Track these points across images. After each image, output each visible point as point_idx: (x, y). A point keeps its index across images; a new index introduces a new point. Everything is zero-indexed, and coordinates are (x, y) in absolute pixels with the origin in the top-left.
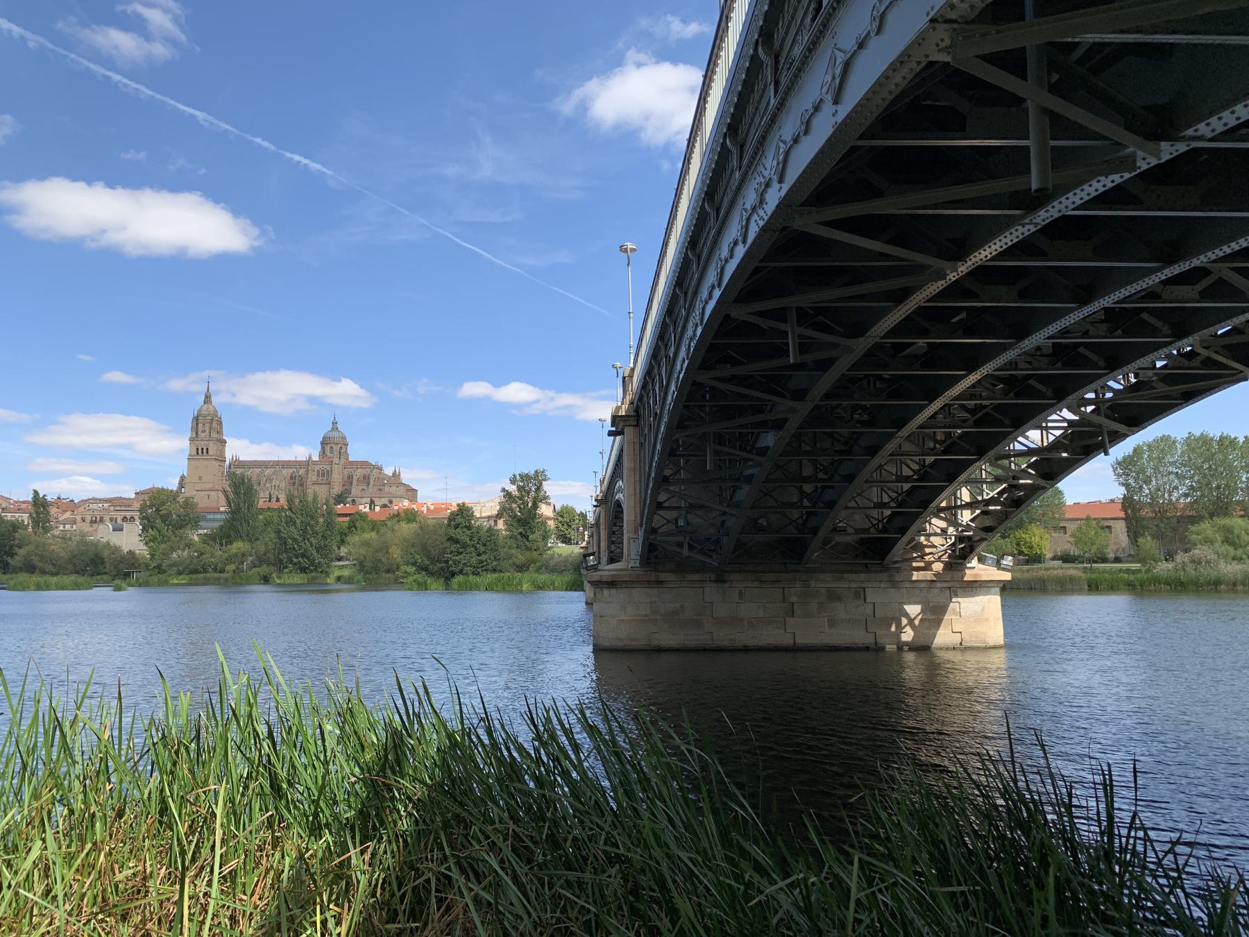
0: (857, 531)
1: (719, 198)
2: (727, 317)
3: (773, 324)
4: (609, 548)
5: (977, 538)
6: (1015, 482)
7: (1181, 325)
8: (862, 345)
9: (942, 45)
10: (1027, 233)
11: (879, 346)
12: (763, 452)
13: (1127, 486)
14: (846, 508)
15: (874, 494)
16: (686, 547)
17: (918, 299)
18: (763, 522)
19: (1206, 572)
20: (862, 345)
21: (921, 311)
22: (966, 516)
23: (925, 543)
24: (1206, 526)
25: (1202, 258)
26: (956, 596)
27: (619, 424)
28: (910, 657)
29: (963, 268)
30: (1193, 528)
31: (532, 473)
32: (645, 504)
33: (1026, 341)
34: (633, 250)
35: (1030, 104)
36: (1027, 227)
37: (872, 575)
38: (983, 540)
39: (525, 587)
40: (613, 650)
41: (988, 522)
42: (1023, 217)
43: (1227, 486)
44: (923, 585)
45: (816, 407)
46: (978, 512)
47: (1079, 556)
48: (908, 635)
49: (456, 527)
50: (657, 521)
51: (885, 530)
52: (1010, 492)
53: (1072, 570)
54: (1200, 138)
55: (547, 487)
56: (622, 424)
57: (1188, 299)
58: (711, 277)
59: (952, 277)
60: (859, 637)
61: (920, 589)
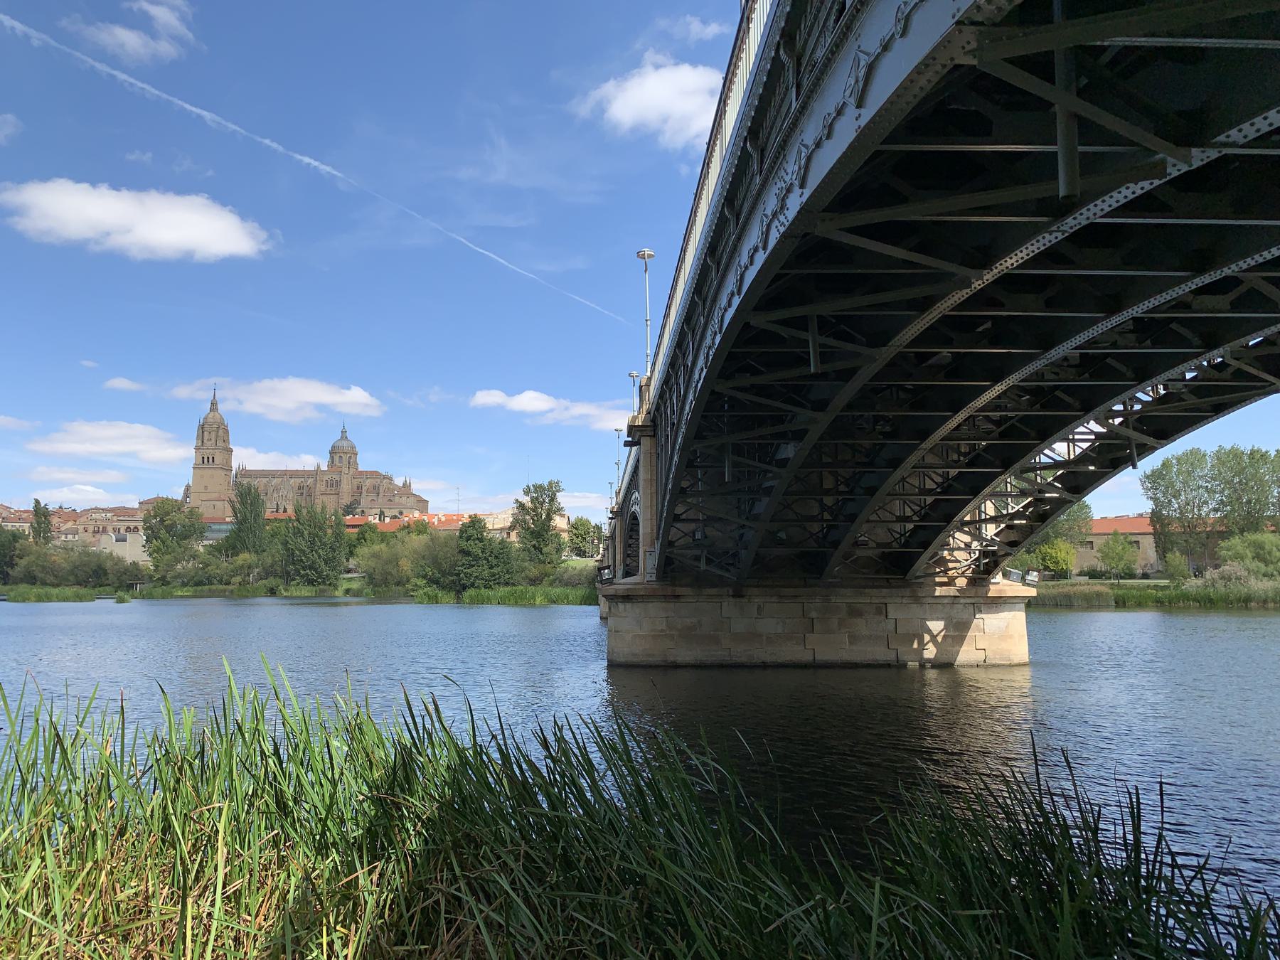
0: (879, 545)
2: (747, 325)
4: (624, 561)
5: (1002, 553)
6: (1041, 496)
7: (1211, 336)
8: (886, 353)
9: (968, 48)
11: (901, 356)
12: (783, 463)
13: (1155, 499)
14: (868, 521)
15: (896, 507)
16: (703, 560)
17: (944, 307)
18: (782, 535)
19: (1236, 589)
20: (886, 353)
21: (944, 319)
22: (990, 530)
23: (948, 558)
24: (1236, 541)
25: (1233, 267)
26: (980, 612)
27: (635, 434)
28: (931, 674)
29: (989, 277)
31: (546, 484)
34: (650, 256)
36: (1055, 234)
38: (1008, 555)
39: (538, 601)
41: (1013, 536)
42: (1049, 224)
43: (1258, 501)
44: (946, 601)
46: (1003, 526)
48: (930, 652)
49: (468, 539)
50: (674, 534)
51: (906, 545)
53: (1099, 586)
54: (1234, 145)
55: (561, 497)
56: (638, 434)
57: (1220, 309)
59: (977, 285)
60: (880, 653)
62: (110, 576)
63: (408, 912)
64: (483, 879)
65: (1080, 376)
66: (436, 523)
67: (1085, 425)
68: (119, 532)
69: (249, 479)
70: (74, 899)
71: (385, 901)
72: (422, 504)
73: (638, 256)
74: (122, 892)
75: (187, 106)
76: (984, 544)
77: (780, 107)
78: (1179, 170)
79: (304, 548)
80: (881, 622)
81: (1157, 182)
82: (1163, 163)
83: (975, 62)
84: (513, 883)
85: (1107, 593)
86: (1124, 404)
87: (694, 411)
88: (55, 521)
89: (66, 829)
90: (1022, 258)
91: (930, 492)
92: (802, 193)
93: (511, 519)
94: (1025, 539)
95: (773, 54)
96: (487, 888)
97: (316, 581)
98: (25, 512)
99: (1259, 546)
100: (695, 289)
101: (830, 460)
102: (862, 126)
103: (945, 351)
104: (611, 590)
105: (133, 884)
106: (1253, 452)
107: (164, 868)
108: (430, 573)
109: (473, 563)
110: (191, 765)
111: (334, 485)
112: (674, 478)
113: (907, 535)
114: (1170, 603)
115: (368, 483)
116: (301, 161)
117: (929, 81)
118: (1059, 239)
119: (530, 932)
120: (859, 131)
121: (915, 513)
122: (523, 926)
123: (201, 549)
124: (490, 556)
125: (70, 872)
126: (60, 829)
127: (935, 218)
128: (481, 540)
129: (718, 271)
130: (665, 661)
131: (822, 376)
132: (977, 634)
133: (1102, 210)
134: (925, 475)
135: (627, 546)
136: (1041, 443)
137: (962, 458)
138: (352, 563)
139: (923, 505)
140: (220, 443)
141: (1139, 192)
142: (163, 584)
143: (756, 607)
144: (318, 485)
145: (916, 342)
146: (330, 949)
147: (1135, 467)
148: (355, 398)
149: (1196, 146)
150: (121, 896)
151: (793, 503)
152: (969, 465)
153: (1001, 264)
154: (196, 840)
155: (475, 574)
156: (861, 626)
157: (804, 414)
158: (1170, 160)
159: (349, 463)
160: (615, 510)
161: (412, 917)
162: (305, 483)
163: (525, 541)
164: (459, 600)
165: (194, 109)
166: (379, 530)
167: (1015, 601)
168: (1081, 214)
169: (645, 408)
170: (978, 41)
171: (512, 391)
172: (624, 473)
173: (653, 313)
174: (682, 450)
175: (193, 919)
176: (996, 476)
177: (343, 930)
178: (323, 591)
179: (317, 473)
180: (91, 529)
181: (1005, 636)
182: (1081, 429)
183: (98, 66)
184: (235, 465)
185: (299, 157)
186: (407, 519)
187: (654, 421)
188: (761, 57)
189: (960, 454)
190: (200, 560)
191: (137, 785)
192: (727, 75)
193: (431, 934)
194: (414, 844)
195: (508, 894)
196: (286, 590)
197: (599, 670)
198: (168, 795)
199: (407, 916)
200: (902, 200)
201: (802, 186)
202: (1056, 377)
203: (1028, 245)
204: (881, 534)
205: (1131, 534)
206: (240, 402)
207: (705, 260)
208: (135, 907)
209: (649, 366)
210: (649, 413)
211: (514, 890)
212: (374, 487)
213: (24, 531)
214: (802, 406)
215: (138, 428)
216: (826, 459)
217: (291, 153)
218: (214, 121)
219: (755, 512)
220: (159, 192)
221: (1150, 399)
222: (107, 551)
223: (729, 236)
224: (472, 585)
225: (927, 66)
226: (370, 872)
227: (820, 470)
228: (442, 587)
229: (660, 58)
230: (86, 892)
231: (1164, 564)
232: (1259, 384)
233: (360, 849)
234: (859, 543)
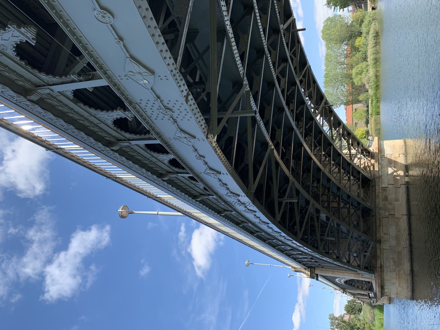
0: (359, 188)
1: (239, 221)
2: (279, 222)
3: (283, 207)
5: (362, 148)
6: (341, 135)
7: (292, 83)
8: (291, 178)
9: (213, 137)
10: (263, 123)
11: (292, 174)
12: (328, 218)
13: (340, 104)
14: (350, 191)
15: (344, 182)
16: (365, 254)
17: (278, 158)
18: (355, 223)
19: (373, 79)
20: (291, 178)
21: (282, 158)
22: (353, 151)
23: (363, 165)
24: (355, 81)
25: (274, 76)
26: (384, 155)
27: (314, 276)
28: (411, 173)
29: (271, 143)
30: (356, 84)
31: (330, 320)
32: (347, 269)
33: (294, 128)
34: (248, 262)
35: (230, 116)
36: (261, 123)
37: (376, 184)
38: (362, 145)
40: (413, 291)
41: (356, 144)
42: (258, 124)
43: (341, 75)
45: (312, 197)
46: (352, 147)
47: (366, 119)
48: (401, 173)
50: (355, 264)
51: (359, 179)
52: (345, 136)
53: (372, 120)
54: (244, 73)
55: (337, 315)
56: (314, 274)
57: (285, 81)
58: (264, 227)
59: (273, 147)
60: (402, 191)
61: (382, 168)
92: (241, 196)
99: (357, 74)
106: (325, 77)
121: (347, 175)
130: (410, 274)
132: (393, 157)
139: (344, 173)
143: (384, 235)
149: (243, 83)
151: (343, 218)
156: (391, 197)
157: (311, 209)
160: (342, 291)
167: (380, 143)
170: (212, 134)
182: (319, 121)
187: (309, 267)
204: (355, 188)
205: (352, 111)
210: (305, 269)
214: (307, 210)
219: (346, 232)
227: (331, 208)
232: (307, 71)
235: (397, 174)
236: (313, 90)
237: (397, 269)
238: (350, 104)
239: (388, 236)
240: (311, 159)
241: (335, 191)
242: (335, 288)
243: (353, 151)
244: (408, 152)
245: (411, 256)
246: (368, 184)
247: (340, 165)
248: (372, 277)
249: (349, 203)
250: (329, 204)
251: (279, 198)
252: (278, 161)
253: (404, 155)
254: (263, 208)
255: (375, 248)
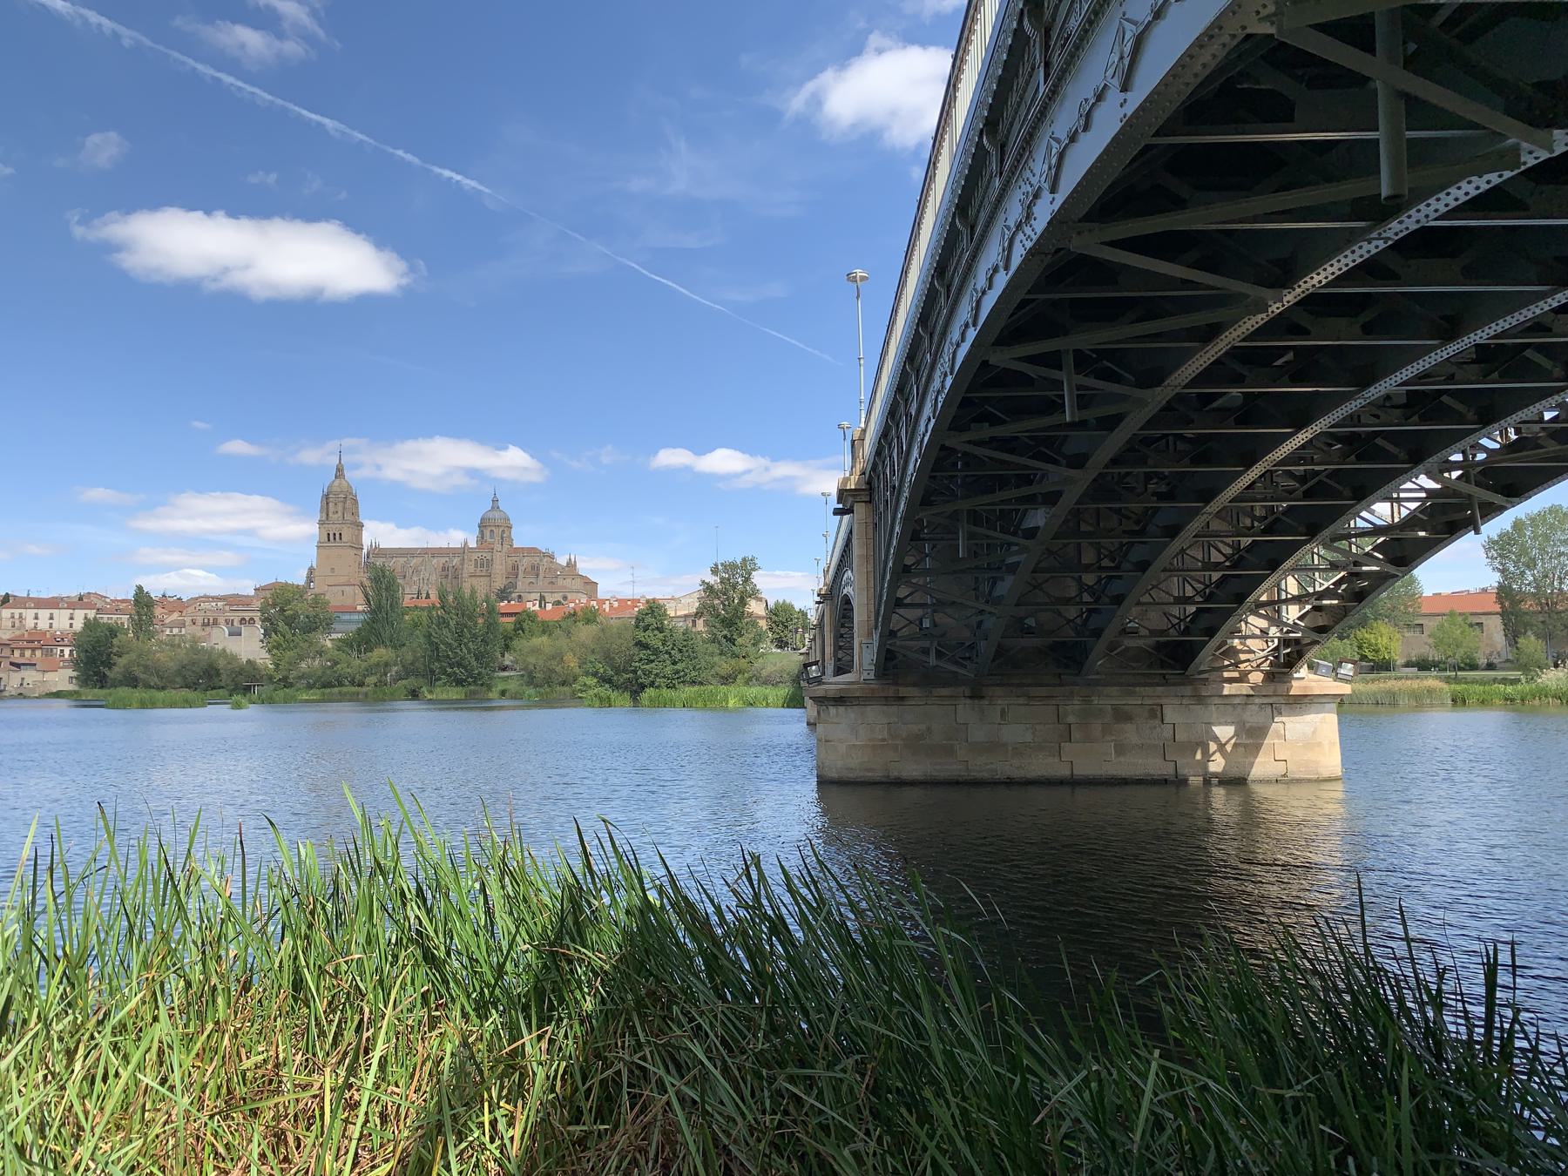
0: (1153, 633)
2: (985, 364)
5: (1307, 641)
6: (1356, 569)
9: (1264, 12)
10: (1374, 251)
11: (1179, 398)
12: (1032, 533)
13: (1503, 571)
14: (1139, 603)
15: (1174, 586)
18: (1031, 622)
21: (1234, 353)
23: (1239, 647)
26: (1280, 714)
27: (847, 501)
28: (1219, 794)
29: (1290, 298)
34: (863, 279)
36: (1375, 243)
39: (731, 703)
41: (1321, 620)
42: (1369, 230)
44: (1237, 701)
46: (1308, 607)
48: (1217, 765)
49: (646, 629)
50: (896, 622)
51: (1187, 632)
55: (758, 579)
56: (850, 499)
59: (1275, 308)
60: (1155, 766)
61: (1233, 705)
62: (224, 677)
63: (584, 1084)
64: (673, 1046)
65: (1406, 419)
66: (607, 610)
67: (1414, 480)
68: (232, 625)
69: (384, 560)
70: (193, 1067)
71: (556, 1071)
72: (590, 586)
73: (848, 279)
74: (248, 1058)
75: (305, 112)
76: (1285, 629)
77: (1025, 91)
78: (1536, 158)
79: (450, 641)
80: (1155, 728)
81: (1507, 174)
82: (1516, 150)
83: (1272, 30)
84: (708, 1051)
85: (1441, 690)
86: (1464, 452)
87: (920, 471)
88: (158, 611)
89: (182, 983)
90: (1333, 273)
91: (1217, 566)
92: (1054, 199)
93: (697, 604)
94: (1337, 623)
95: (1015, 25)
96: (677, 1056)
97: (465, 681)
98: (123, 601)
100: (919, 319)
101: (1090, 529)
102: (1129, 114)
103: (1235, 391)
104: (819, 690)
105: (260, 1049)
107: (296, 1029)
108: (602, 670)
109: (652, 658)
110: (324, 908)
111: (485, 565)
112: (896, 554)
113: (1188, 619)
114: (1523, 700)
115: (525, 562)
116: (441, 174)
117: (1214, 56)
118: (1380, 248)
119: (730, 1110)
120: (1125, 120)
121: (1198, 593)
122: (722, 1103)
123: (329, 644)
124: (673, 649)
125: (187, 1035)
126: (175, 985)
127: (1220, 227)
128: (661, 630)
129: (948, 297)
131: (1081, 425)
132: (1276, 741)
133: (1436, 211)
134: (1210, 545)
135: (839, 636)
136: (1356, 504)
137: (1256, 524)
138: (508, 659)
139: (1207, 583)
140: (348, 517)
141: (1484, 187)
142: (285, 686)
143: (999, 708)
144: (466, 566)
145: (1195, 382)
146: (493, 1128)
147: (1477, 532)
148: (513, 460)
150: (247, 1064)
152: (1265, 532)
153: (1306, 282)
154: (333, 997)
155: (655, 672)
157: (1056, 475)
158: (1525, 145)
159: (502, 538)
161: (590, 1089)
162: (449, 562)
163: (715, 631)
164: (636, 702)
165: (313, 116)
166: (539, 619)
168: (1409, 217)
169: (859, 467)
171: (701, 450)
172: (834, 548)
173: (867, 349)
174: (905, 519)
175: (331, 1091)
176: (1301, 544)
177: (507, 1106)
178: (474, 693)
179: (464, 551)
180: (199, 621)
181: (1311, 744)
182: (1409, 485)
183: (200, 67)
184: (367, 540)
185: (437, 170)
186: (572, 605)
187: (869, 483)
188: (1000, 30)
189: (1254, 518)
190: (328, 656)
191: (263, 931)
192: (957, 52)
193: (611, 1112)
194: (588, 1005)
195: (702, 1063)
196: (430, 692)
197: (808, 790)
198: (299, 942)
199: (583, 1089)
200: (1179, 204)
201: (1053, 190)
202: (1377, 421)
203: (1341, 257)
204: (1155, 620)
205: (1472, 614)
206: (379, 468)
207: (932, 283)
208: (263, 1076)
209: (863, 416)
210: (864, 473)
211: (709, 1059)
212: (533, 567)
213: (122, 624)
214: (1055, 462)
215: (257, 500)
216: (1084, 527)
217: (428, 166)
218: (337, 130)
219: (996, 593)
220: (284, 219)
221: (1498, 446)
222: (220, 647)
223: (962, 253)
224: (652, 684)
225: (1211, 37)
226: (540, 1038)
228: (615, 687)
229: (886, 42)
230: (207, 1059)
231: (1515, 651)
233: (526, 1009)
234: (1127, 630)
235: (1211, 752)
236: (1548, 453)
237: (899, 742)
238: (1502, 603)
239: (999, 721)
240: (1249, 464)
241: (1137, 554)
242: (828, 571)
243: (1292, 613)
244: (1294, 790)
245: (932, 783)
246: (1172, 662)
247: (1234, 567)
248: (865, 673)
249: (1096, 602)
250: (1089, 535)
251: (1077, 352)
252: (1223, 337)
253: (1284, 776)
254: (1021, 295)
255: (953, 681)
